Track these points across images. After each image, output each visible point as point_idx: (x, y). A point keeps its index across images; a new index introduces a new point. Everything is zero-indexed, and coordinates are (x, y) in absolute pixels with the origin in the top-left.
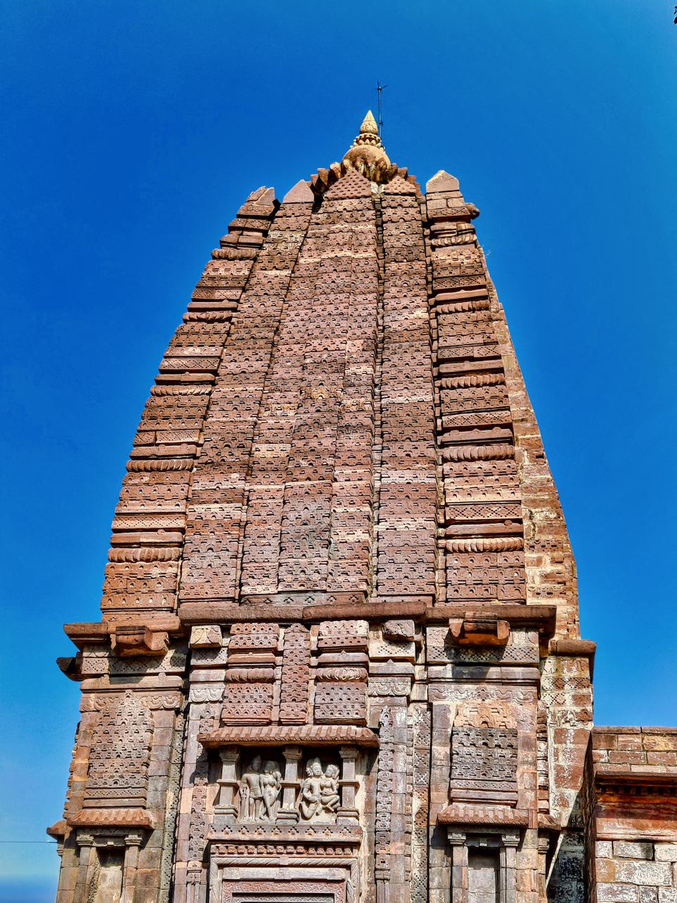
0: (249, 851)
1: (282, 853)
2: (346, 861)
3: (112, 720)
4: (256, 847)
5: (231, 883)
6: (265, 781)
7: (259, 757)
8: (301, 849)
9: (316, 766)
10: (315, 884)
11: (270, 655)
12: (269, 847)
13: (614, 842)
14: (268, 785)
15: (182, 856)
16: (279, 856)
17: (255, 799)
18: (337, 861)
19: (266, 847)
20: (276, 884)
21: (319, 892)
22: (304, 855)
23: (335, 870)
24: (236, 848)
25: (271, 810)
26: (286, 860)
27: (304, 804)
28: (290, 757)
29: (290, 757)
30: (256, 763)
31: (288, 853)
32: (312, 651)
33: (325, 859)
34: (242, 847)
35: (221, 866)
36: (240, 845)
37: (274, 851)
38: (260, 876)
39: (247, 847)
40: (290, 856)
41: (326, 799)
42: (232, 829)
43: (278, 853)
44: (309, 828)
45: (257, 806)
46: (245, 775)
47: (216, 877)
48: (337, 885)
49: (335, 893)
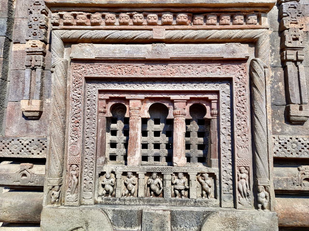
1: (154, 24)
2: (248, 33)
4: (117, 17)
5: (82, 65)
8: (182, 17)
10: (204, 66)
13: (287, 54)
15: (20, 37)
16: (151, 27)
18: (237, 33)
20: (147, 66)
21: (177, 76)
22: (189, 27)
23: (234, 46)
26: (161, 33)
31: (164, 24)
33: (219, 31)
34: (98, 15)
35: (68, 42)
36: (93, 12)
37: (145, 22)
38: (124, 55)
40: (167, 27)
43: (149, 24)
47: (59, 57)
48: (236, 66)
49: (233, 77)
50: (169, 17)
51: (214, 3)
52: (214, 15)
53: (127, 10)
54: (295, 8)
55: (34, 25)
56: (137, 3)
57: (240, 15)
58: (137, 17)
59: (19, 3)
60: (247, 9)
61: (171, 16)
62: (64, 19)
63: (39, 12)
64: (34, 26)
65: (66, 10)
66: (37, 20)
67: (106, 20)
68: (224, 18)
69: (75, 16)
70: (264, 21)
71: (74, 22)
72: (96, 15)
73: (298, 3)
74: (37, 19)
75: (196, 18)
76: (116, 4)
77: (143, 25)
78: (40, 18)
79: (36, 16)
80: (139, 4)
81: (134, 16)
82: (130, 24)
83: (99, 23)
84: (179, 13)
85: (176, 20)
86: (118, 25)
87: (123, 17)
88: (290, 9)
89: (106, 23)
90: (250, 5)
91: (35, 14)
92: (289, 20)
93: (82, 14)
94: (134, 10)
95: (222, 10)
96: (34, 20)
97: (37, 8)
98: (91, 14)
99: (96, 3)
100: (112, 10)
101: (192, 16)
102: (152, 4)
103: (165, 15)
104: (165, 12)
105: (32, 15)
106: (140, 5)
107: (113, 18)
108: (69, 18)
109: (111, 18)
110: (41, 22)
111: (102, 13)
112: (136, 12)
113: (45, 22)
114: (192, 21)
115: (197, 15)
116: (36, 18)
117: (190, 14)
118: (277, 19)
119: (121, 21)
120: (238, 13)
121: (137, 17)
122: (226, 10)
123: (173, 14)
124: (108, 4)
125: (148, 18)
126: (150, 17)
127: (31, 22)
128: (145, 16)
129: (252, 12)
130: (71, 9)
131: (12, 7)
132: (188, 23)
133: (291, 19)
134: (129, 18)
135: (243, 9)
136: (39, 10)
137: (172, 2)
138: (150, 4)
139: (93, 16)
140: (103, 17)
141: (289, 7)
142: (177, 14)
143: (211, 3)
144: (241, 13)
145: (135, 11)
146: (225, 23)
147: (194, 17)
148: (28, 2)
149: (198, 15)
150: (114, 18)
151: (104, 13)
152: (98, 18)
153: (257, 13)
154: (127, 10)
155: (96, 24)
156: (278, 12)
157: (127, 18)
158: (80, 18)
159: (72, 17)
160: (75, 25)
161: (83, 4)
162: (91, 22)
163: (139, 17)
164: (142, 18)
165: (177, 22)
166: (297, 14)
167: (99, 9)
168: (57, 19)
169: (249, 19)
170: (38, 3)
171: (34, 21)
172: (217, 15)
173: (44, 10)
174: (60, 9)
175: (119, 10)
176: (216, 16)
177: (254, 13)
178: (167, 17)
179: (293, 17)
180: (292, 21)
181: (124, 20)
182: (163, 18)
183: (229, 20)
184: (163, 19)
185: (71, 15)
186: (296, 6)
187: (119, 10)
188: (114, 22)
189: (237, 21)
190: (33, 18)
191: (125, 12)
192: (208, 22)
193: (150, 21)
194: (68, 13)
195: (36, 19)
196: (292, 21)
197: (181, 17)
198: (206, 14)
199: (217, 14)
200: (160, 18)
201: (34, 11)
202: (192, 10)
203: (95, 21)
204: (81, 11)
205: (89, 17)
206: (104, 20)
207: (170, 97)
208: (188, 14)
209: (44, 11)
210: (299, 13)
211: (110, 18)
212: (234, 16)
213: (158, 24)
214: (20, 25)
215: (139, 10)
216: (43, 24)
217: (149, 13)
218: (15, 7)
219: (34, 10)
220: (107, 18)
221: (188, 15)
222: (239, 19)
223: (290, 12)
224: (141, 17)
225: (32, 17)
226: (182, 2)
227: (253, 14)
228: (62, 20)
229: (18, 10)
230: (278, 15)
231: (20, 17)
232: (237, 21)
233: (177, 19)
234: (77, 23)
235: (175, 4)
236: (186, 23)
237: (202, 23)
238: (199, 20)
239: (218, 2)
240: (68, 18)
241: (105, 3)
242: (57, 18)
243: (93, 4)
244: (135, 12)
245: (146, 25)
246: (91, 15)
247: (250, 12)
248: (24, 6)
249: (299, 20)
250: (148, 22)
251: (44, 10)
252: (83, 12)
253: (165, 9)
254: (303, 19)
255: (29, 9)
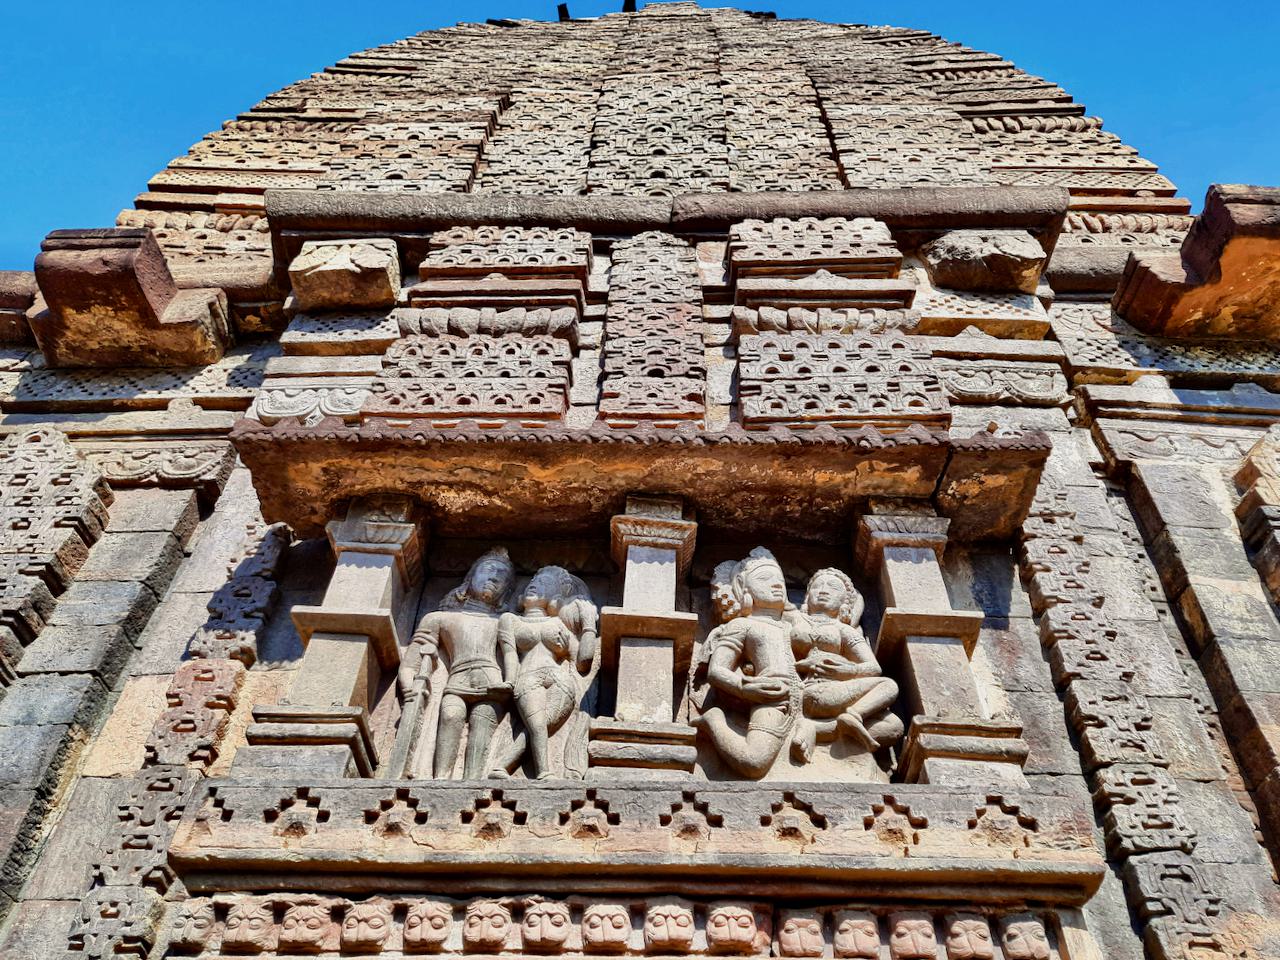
0: (415, 935)
3: (141, 830)
4: (459, 913)
6: (524, 638)
7: (505, 554)
9: (763, 572)
11: (568, 247)
12: (539, 907)
14: (540, 648)
17: (471, 702)
19: (518, 913)
24: (338, 914)
25: (550, 751)
27: (717, 718)
28: (649, 534)
29: (649, 534)
30: (490, 571)
32: (706, 289)
34: (378, 909)
36: (360, 896)
39: (400, 913)
41: (829, 691)
42: (324, 805)
44: (778, 798)
45: (480, 732)
46: (431, 619)
50: (675, 918)
51: (856, 867)
52: (862, 910)
53: (501, 886)
54: (1186, 878)
55: (95, 935)
56: (547, 861)
57: (975, 916)
58: (540, 916)
59: (64, 839)
60: (996, 895)
61: (684, 913)
62: (229, 926)
63: (137, 877)
64: (94, 939)
65: (248, 887)
66: (115, 915)
67: (410, 927)
68: (909, 929)
69: (279, 911)
70: (1079, 943)
71: (271, 937)
72: (369, 907)
73: (1194, 860)
74: (118, 912)
75: (789, 924)
76: (460, 864)
77: (567, 951)
78: (130, 904)
79: (120, 895)
80: (553, 864)
81: (529, 911)
82: (509, 946)
83: (376, 941)
84: (719, 903)
85: (705, 928)
86: (456, 951)
87: (481, 918)
88: (1166, 881)
89: (405, 941)
90: (1003, 880)
91: (115, 888)
92: (1178, 929)
93: (312, 903)
94: (530, 886)
95: (891, 893)
96: (104, 914)
97: (133, 860)
98: (349, 902)
99: (380, 860)
100: (441, 886)
101: (772, 912)
102: (606, 866)
103: (657, 910)
104: (662, 895)
105: (102, 893)
106: (556, 870)
107: (438, 921)
108: (254, 922)
109: (431, 919)
110: (128, 924)
111: (398, 898)
112: (541, 893)
113: (149, 921)
114: (774, 934)
115: (791, 912)
116: (114, 904)
117: (764, 905)
118: (1128, 922)
119: (475, 935)
120: (963, 909)
121: (540, 916)
122: (909, 893)
123: (691, 904)
124: (427, 863)
125: (588, 920)
126: (595, 920)
127: (86, 921)
128: (577, 913)
129: (1018, 904)
130: (270, 883)
131: (36, 832)
132: (756, 943)
133: (1187, 924)
134: (509, 918)
135: (976, 894)
136: (137, 869)
137: (685, 861)
138: (598, 865)
139: (355, 914)
140: (400, 913)
141: (1163, 877)
142: (710, 906)
143: (843, 870)
144: (974, 910)
145: (533, 892)
146: (914, 952)
147: (780, 917)
148: (103, 834)
149: (796, 912)
150: (445, 920)
151: (405, 900)
152: (377, 921)
153: (1041, 911)
154: (501, 886)
155: (363, 948)
156: (1121, 892)
157: (498, 920)
158: (301, 922)
159: (268, 916)
160: (269, 951)
161: (326, 862)
162: (342, 939)
163: (551, 916)
164: (562, 919)
165: (709, 939)
166: (1205, 904)
167: (386, 883)
168: (198, 926)
169: (1011, 937)
170: (143, 842)
171: (100, 919)
172: (873, 912)
173: (157, 868)
174: (226, 882)
175: (469, 886)
176: (873, 917)
177: (1025, 911)
178: (666, 917)
179: (1192, 919)
180: (1195, 934)
181: (484, 930)
182: (651, 920)
183: (929, 937)
184: (648, 925)
185: (265, 908)
186: (1187, 871)
187: (469, 886)
188: (441, 937)
189: (966, 944)
190: (100, 903)
191: (494, 895)
192: (842, 942)
193: (597, 936)
194: (255, 897)
195: (113, 910)
196: (1195, 934)
197: (728, 918)
198: (828, 908)
199: (876, 907)
200: (637, 923)
201: (114, 873)
202: (770, 890)
203: (362, 937)
204: (310, 892)
205: (338, 914)
206: (401, 926)
207: (683, 518)
208: (753, 904)
209: (159, 874)
210: (1212, 902)
211: (426, 922)
212: (948, 919)
213: (629, 947)
214: (33, 932)
215: (553, 887)
216: (135, 931)
217: (594, 900)
218: (45, 834)
219: (116, 868)
220: (415, 920)
221: (757, 911)
222: (973, 935)
223: (1171, 895)
224: (558, 918)
225: (101, 899)
226: (729, 862)
227: (1023, 916)
228: (220, 925)
229: (52, 864)
230: (1125, 904)
231: (48, 897)
232: (966, 944)
233: (711, 926)
234: (282, 943)
235: (699, 866)
236: (750, 947)
237: (818, 949)
238: (803, 931)
239: (872, 863)
240: (250, 919)
241: (416, 860)
242: (199, 922)
243: (364, 862)
244: (536, 897)
245: (577, 951)
246: (350, 906)
247: (1007, 904)
248: (78, 850)
249: (1217, 929)
250: (586, 938)
251: (157, 868)
252: (320, 892)
253: (659, 885)
254: (1234, 924)
255: (97, 867)
